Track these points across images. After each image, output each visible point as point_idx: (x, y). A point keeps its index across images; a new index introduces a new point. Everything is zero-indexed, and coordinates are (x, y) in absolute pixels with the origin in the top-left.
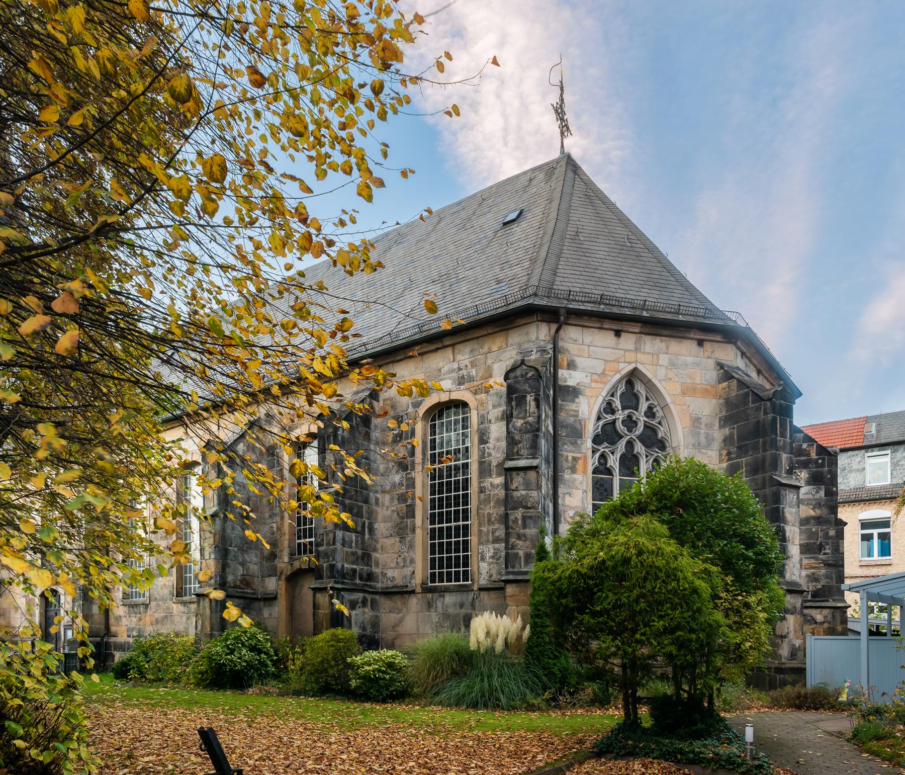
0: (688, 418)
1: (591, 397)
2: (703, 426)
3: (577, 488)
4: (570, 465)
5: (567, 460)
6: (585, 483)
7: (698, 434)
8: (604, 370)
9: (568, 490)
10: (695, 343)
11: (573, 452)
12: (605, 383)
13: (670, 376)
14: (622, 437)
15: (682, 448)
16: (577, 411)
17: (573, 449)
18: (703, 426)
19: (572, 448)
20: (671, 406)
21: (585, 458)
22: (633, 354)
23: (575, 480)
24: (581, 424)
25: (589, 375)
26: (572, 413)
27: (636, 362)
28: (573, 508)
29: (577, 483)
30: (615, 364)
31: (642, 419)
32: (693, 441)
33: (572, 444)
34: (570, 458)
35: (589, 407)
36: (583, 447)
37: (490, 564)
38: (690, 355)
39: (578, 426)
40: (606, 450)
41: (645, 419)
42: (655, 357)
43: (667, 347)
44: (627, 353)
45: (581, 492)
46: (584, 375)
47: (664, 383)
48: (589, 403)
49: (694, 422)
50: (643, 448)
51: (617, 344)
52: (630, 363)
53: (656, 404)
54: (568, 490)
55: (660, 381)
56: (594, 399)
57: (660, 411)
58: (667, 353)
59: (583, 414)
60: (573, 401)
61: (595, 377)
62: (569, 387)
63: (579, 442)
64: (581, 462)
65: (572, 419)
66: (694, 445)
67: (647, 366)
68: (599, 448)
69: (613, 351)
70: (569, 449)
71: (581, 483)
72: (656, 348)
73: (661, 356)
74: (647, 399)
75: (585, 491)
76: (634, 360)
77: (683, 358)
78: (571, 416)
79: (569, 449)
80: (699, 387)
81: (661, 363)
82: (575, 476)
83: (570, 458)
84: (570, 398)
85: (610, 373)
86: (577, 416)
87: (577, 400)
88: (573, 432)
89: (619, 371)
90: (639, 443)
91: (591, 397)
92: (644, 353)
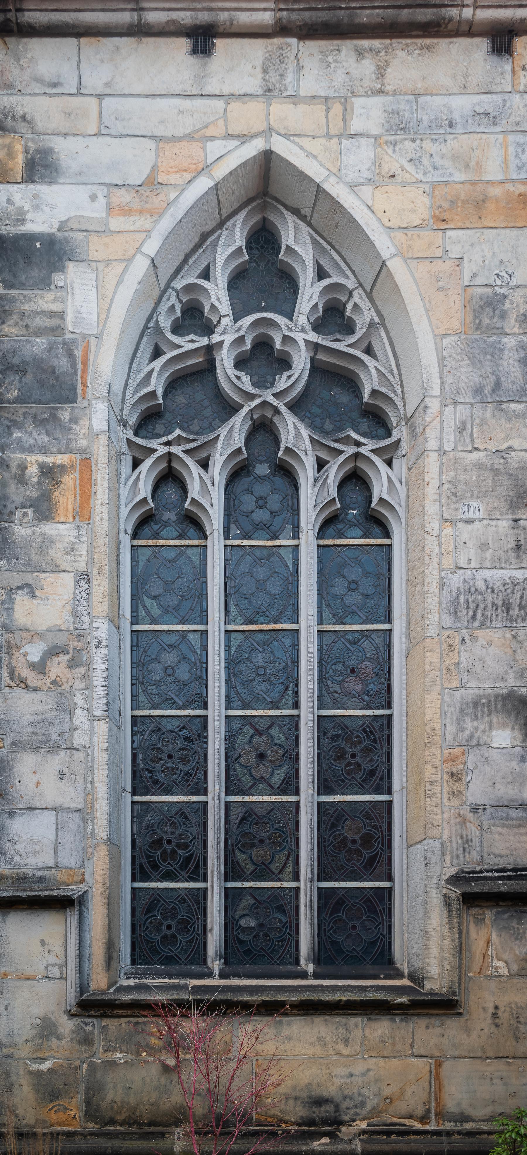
0: (455, 302)
1: (108, 262)
2: (511, 324)
3: (57, 569)
4: (32, 493)
5: (21, 479)
6: (83, 549)
7: (496, 351)
8: (155, 169)
9: (28, 578)
10: (483, 44)
11: (44, 450)
12: (158, 214)
13: (390, 165)
14: (233, 409)
15: (434, 405)
16: (61, 315)
17: (44, 439)
18: (511, 324)
19: (41, 437)
20: (395, 266)
21: (86, 464)
22: (255, 107)
23: (48, 541)
24: (70, 355)
25: (101, 192)
26: (39, 322)
27: (269, 131)
28: (40, 634)
29: (56, 553)
30: (194, 149)
31: (299, 337)
32: (475, 379)
33: (39, 422)
34: (33, 471)
35: (101, 297)
36: (79, 431)
37: (184, 1140)
38: (464, 90)
39: (62, 364)
40: (176, 450)
41: (313, 337)
42: (337, 108)
43: (381, 72)
44: (235, 106)
45: (69, 579)
46: (82, 193)
47: (366, 191)
48: (98, 285)
49: (477, 314)
50: (305, 433)
51: (201, 77)
52: (244, 138)
53: (350, 283)
54: (28, 578)
55: (353, 186)
56: (118, 268)
57: (365, 304)
58: (381, 92)
59: (78, 320)
60: (45, 284)
61: (123, 197)
62: (31, 238)
63: (65, 414)
64: (69, 481)
65: (40, 344)
66: (478, 391)
67: (305, 142)
68: (153, 444)
69: (187, 103)
70: (28, 441)
71: (71, 550)
72: (340, 77)
73: (357, 103)
74: (321, 274)
75: (85, 577)
76: (259, 126)
77: (439, 101)
78: (38, 332)
79: (28, 441)
80: (496, 191)
81: (356, 125)
82: (49, 529)
83: (33, 471)
84: (35, 273)
85: (174, 178)
86: (59, 330)
87: (58, 279)
88: (42, 384)
89: (205, 169)
90: (290, 418)
91: (108, 262)
92: (294, 99)
